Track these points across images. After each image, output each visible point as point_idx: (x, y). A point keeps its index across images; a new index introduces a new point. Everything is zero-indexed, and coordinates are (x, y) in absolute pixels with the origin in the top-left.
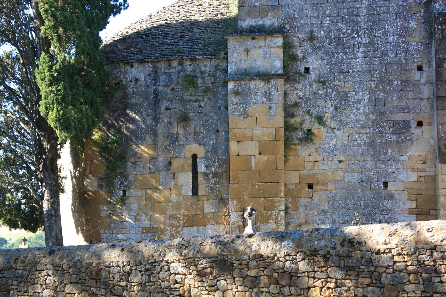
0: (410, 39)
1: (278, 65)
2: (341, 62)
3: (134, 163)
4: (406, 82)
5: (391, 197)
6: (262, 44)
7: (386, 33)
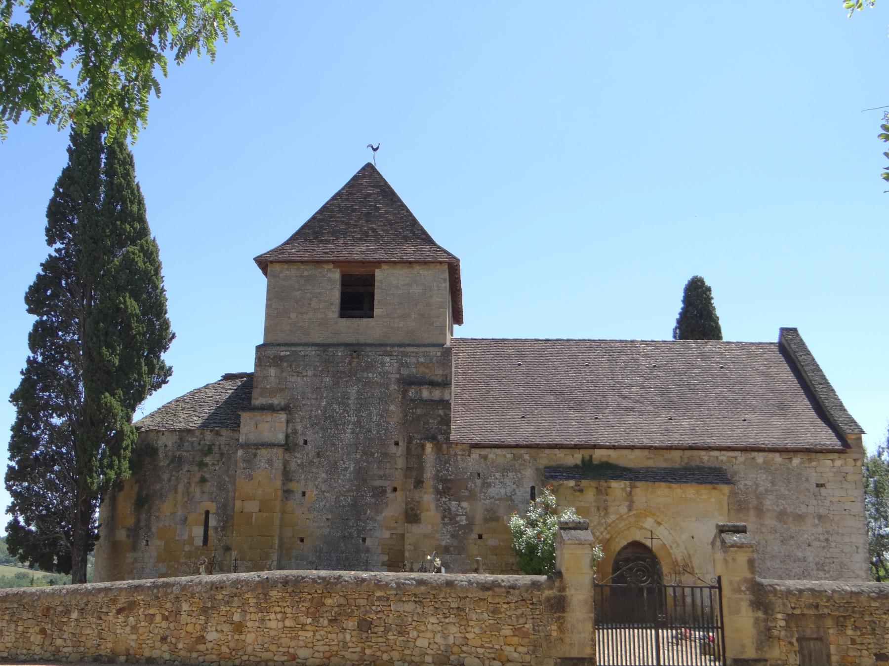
0: (390, 420)
1: (281, 437)
2: (333, 436)
3: (157, 517)
4: (385, 455)
5: (368, 550)
6: (269, 419)
7: (370, 414)
